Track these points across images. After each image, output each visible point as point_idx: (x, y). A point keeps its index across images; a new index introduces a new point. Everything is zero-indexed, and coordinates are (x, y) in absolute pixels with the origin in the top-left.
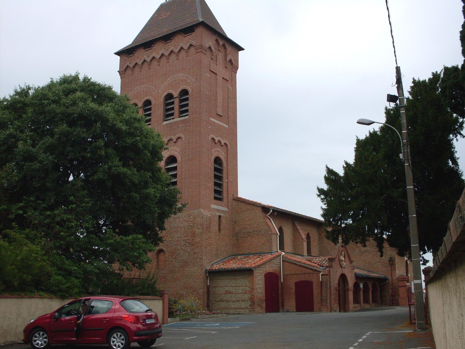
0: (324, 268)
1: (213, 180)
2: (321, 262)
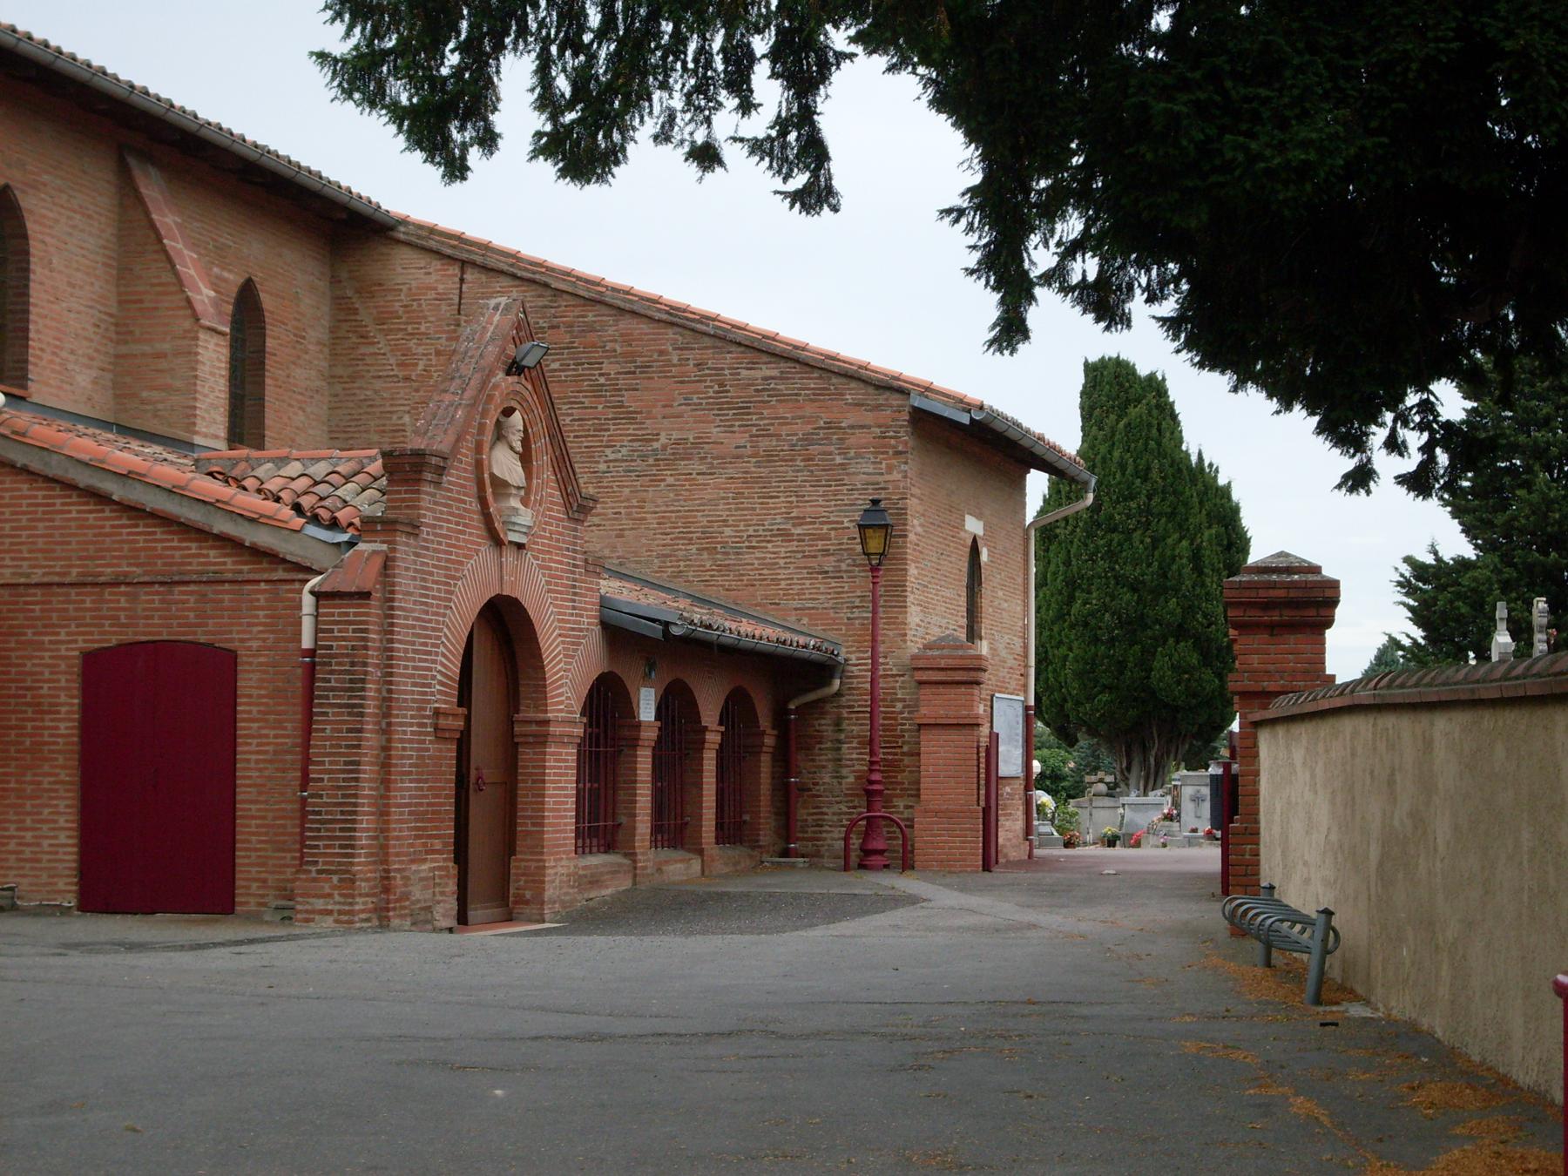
0: (345, 537)
2: (322, 489)
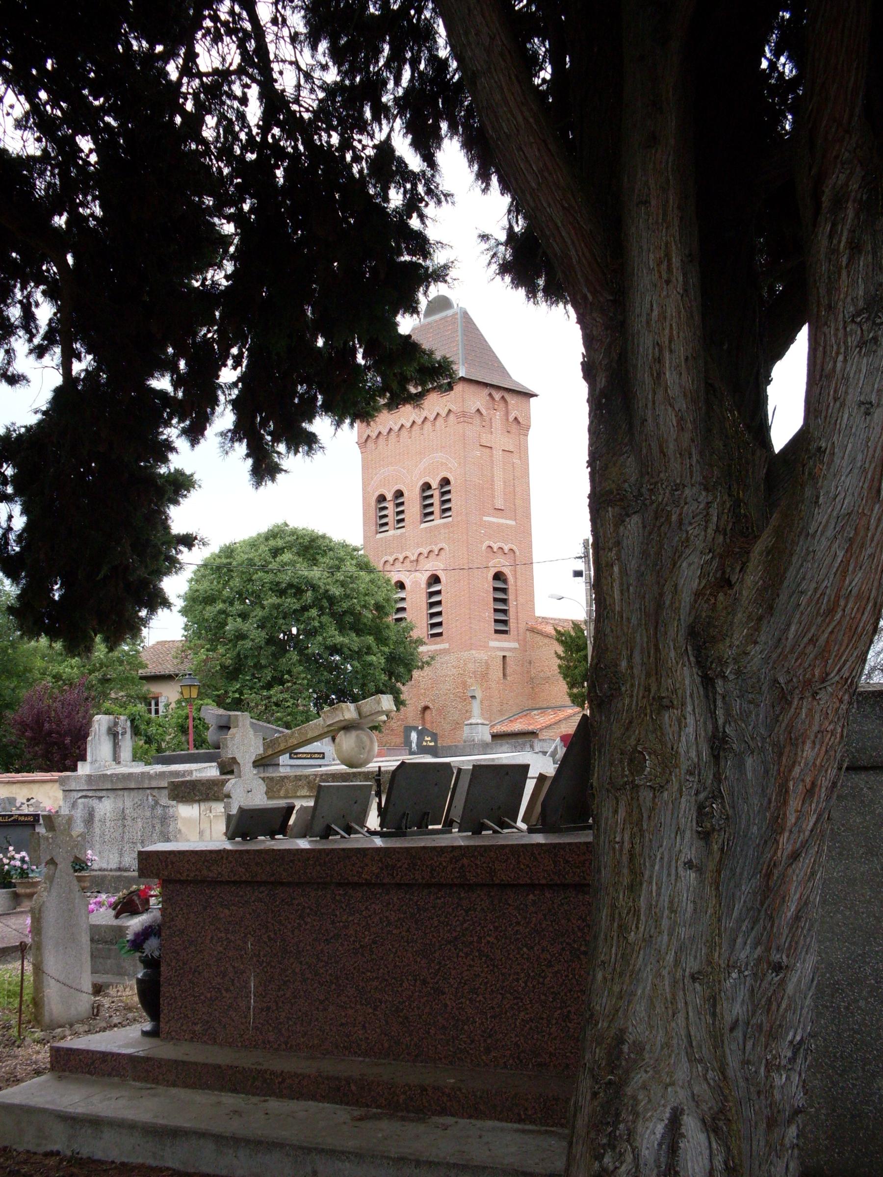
1: (492, 605)
